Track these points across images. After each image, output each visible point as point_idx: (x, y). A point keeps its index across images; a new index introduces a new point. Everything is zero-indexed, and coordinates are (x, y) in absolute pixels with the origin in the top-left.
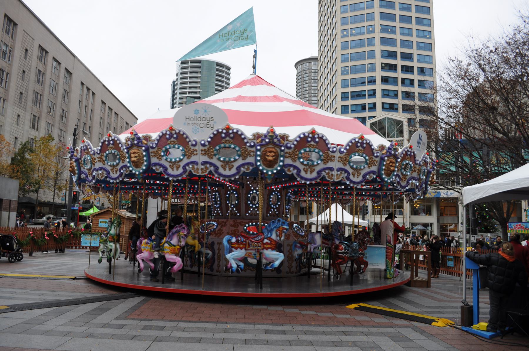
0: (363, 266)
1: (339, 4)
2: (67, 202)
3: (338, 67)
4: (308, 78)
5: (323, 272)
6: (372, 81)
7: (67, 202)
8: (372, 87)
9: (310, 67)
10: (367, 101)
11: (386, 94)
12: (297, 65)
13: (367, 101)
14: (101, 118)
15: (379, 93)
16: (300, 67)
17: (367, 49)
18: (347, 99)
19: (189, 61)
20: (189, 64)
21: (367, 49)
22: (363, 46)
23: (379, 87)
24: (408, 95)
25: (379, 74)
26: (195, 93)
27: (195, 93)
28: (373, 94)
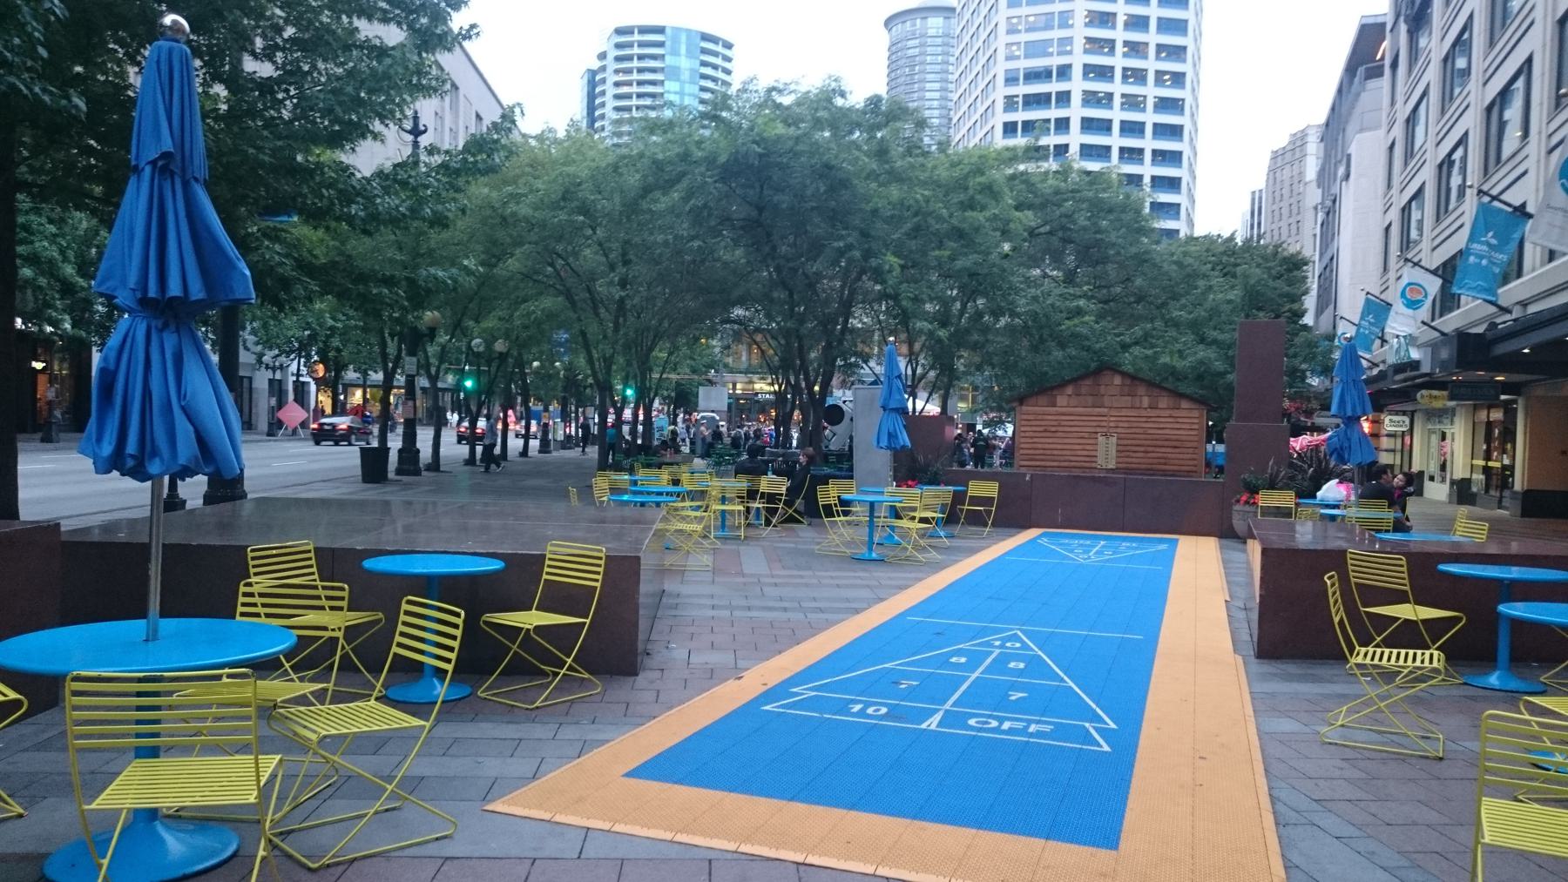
0: (1106, 50)
1: (1004, 12)
2: (1500, 327)
3: (1001, 92)
4: (917, 50)
5: (89, 333)
6: (1064, 72)
7: (1500, 327)
8: (1062, 86)
9: (923, 32)
10: (1053, 87)
11: (1091, 99)
12: (889, 22)
13: (1053, 87)
14: (436, 114)
15: (1076, 99)
16: (898, 29)
17: (1057, 34)
18: (1009, 76)
19: (633, 27)
20: (637, 37)
21: (1057, 34)
22: (1049, 27)
23: (1077, 85)
24: (1132, 102)
25: (1078, 60)
26: (653, 70)
27: (653, 70)
28: (1063, 125)
